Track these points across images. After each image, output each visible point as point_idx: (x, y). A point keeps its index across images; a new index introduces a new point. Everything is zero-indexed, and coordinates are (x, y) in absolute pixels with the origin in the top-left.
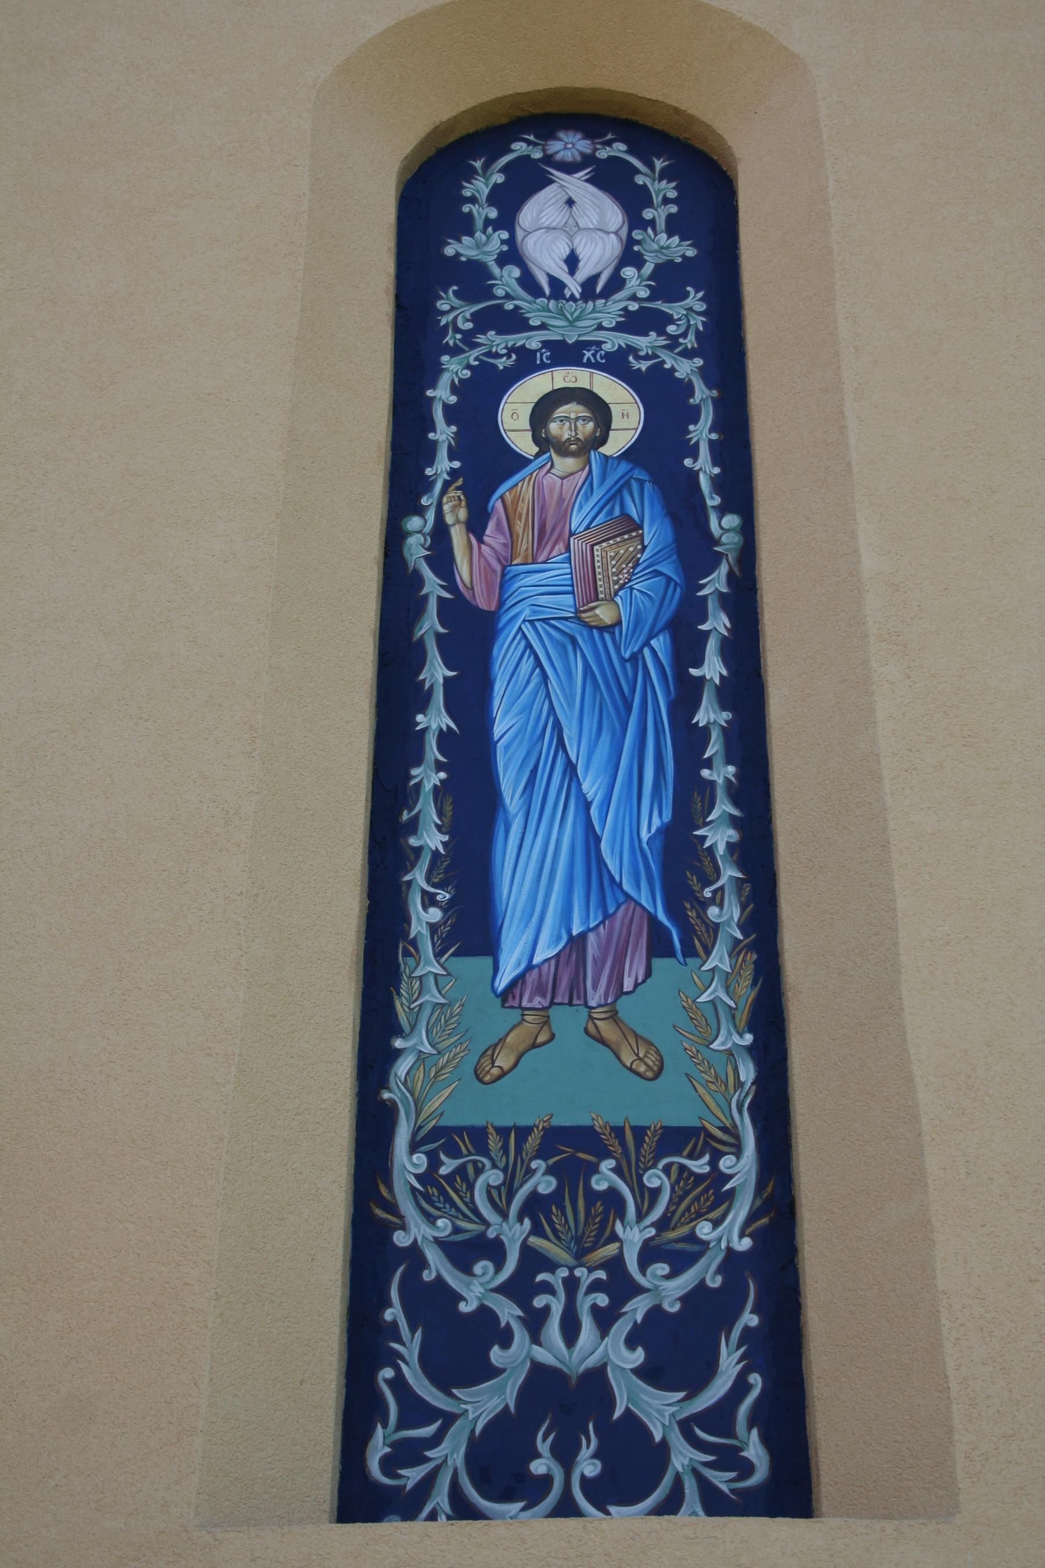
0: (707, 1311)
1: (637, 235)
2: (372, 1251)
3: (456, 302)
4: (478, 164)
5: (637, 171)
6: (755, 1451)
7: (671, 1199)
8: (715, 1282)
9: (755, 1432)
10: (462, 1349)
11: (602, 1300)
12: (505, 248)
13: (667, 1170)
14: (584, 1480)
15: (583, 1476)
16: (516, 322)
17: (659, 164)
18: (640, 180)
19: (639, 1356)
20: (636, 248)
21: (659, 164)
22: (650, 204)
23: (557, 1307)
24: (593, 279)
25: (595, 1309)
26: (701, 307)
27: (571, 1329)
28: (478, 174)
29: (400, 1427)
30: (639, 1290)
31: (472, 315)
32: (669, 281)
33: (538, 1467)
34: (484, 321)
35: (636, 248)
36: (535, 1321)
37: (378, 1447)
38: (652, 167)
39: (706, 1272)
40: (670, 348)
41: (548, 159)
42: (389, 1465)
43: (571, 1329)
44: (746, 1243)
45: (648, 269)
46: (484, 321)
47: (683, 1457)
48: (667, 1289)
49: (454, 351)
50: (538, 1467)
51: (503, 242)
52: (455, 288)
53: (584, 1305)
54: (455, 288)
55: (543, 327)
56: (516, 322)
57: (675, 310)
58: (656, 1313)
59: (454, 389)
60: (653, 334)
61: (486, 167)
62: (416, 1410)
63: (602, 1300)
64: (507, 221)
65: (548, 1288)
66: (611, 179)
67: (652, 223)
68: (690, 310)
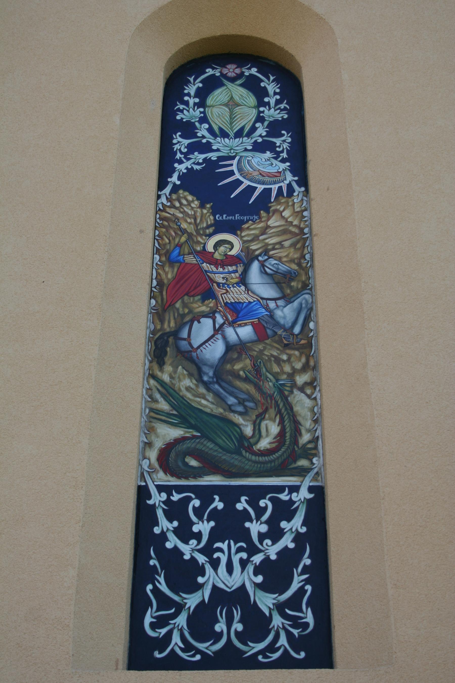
0: (288, 558)
1: (262, 109)
2: (144, 536)
3: (180, 139)
4: (192, 79)
5: (262, 81)
6: (310, 618)
7: (231, 316)
8: (292, 546)
9: (309, 609)
10: (185, 575)
11: (244, 555)
12: (202, 115)
13: (271, 499)
14: (236, 632)
15: (236, 630)
16: (207, 148)
17: (272, 78)
18: (262, 85)
19: (259, 579)
20: (261, 115)
21: (272, 78)
22: (267, 95)
23: (224, 559)
24: (242, 129)
25: (241, 560)
26: (289, 140)
27: (230, 569)
28: (191, 83)
29: (157, 610)
30: (260, 551)
31: (188, 144)
32: (275, 128)
33: (217, 628)
34: (192, 148)
35: (261, 115)
36: (215, 564)
37: (148, 620)
38: (269, 79)
39: (287, 541)
40: (276, 158)
41: (224, 76)
42: (153, 626)
43: (230, 569)
44: (304, 530)
45: (266, 123)
46: (192, 148)
47: (277, 621)
48: (272, 551)
49: (180, 162)
50: (217, 628)
51: (201, 113)
52: (179, 133)
53: (236, 560)
54: (179, 133)
55: (218, 150)
56: (207, 148)
57: (278, 141)
58: (267, 559)
59: (179, 178)
60: (268, 152)
61: (195, 80)
62: (164, 601)
63: (244, 555)
64: (202, 104)
65: (220, 550)
66: (252, 85)
67: (268, 103)
68: (283, 142)
